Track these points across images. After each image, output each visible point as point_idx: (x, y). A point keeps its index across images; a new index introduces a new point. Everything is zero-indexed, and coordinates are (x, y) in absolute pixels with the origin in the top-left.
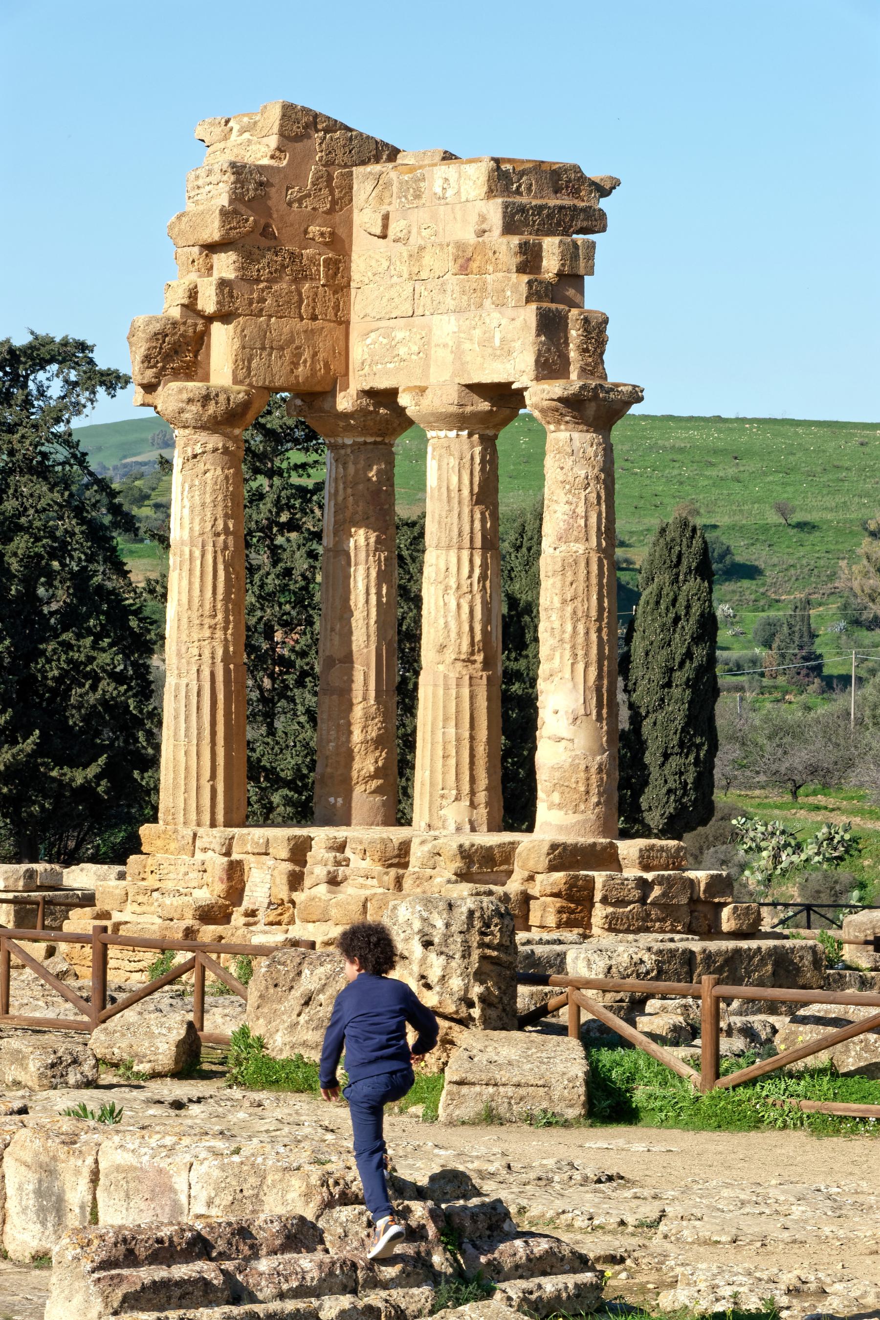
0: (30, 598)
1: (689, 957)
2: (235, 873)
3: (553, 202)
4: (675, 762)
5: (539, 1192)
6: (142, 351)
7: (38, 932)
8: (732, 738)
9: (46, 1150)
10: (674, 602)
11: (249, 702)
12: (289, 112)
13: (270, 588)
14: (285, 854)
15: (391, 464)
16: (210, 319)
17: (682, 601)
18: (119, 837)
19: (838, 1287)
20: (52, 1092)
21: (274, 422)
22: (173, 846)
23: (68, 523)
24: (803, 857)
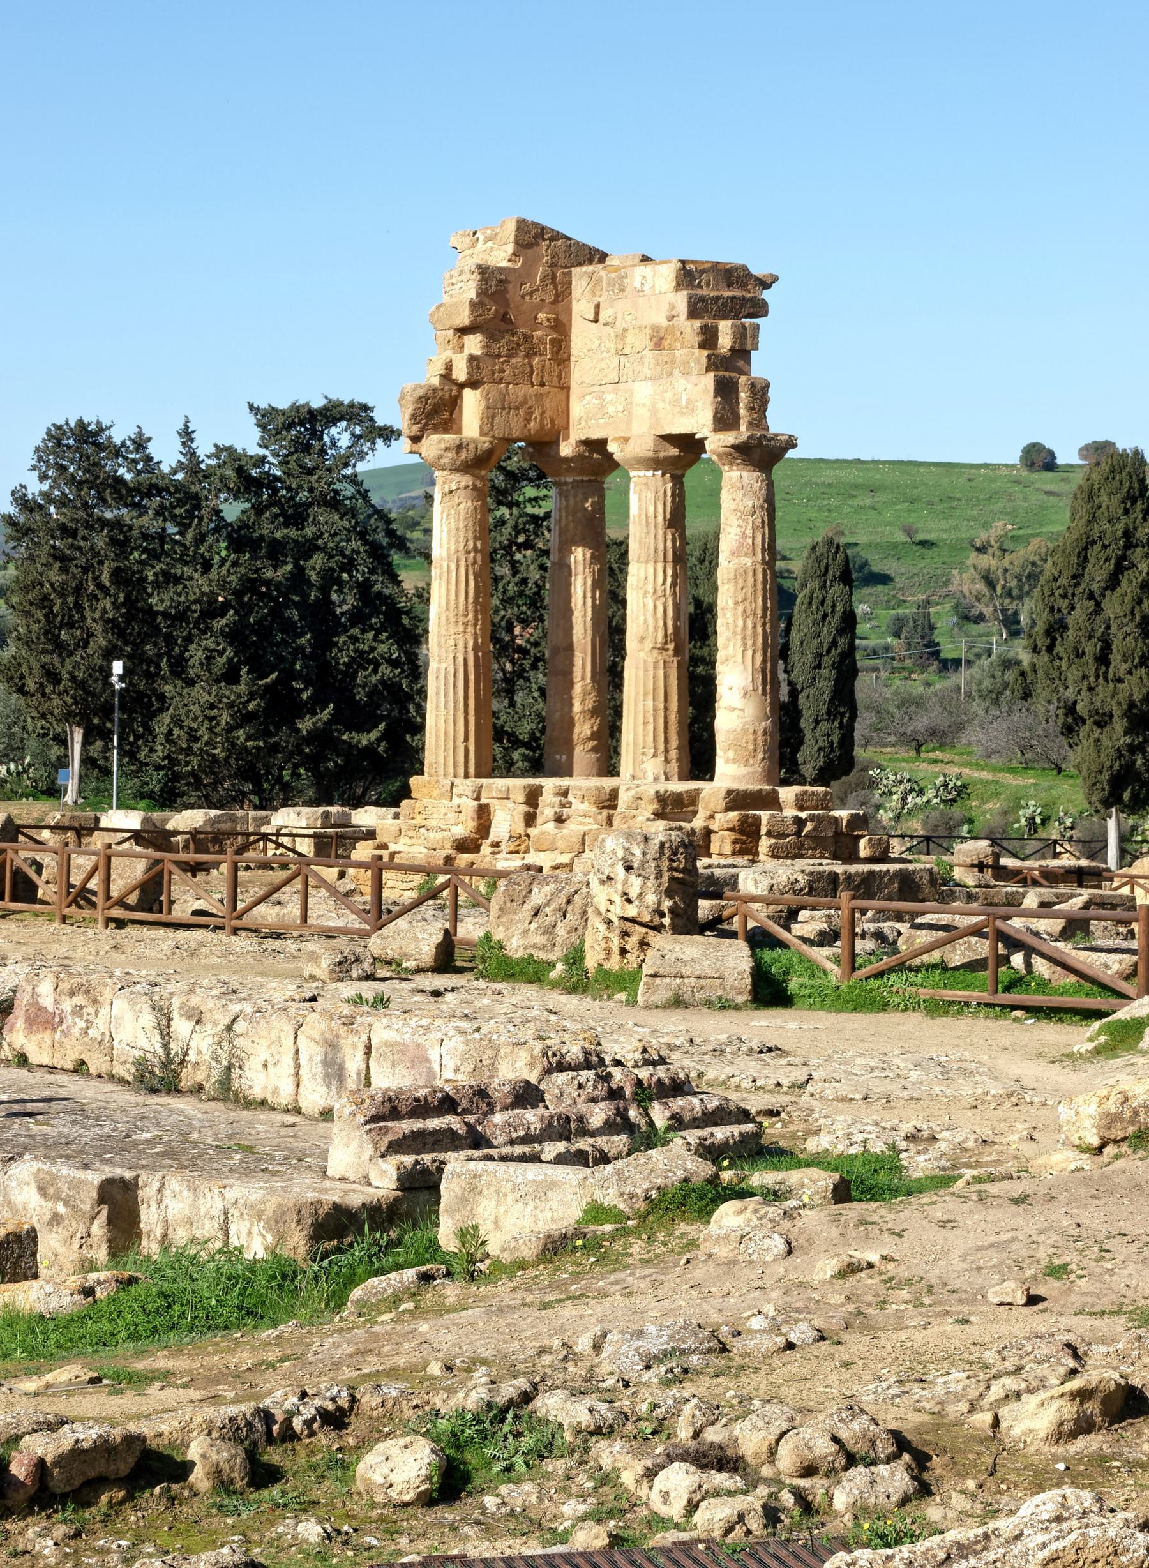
0: (325, 603)
1: (833, 878)
2: (483, 814)
3: (726, 294)
4: (823, 727)
5: (714, 1060)
6: (409, 411)
7: (332, 860)
8: (868, 708)
9: (330, 1029)
10: (823, 602)
11: (495, 681)
12: (522, 225)
13: (511, 594)
14: (522, 799)
15: (602, 497)
16: (462, 386)
17: (829, 601)
18: (395, 786)
19: (946, 1134)
20: (339, 984)
21: (514, 464)
22: (436, 793)
23: (355, 544)
24: (925, 799)
